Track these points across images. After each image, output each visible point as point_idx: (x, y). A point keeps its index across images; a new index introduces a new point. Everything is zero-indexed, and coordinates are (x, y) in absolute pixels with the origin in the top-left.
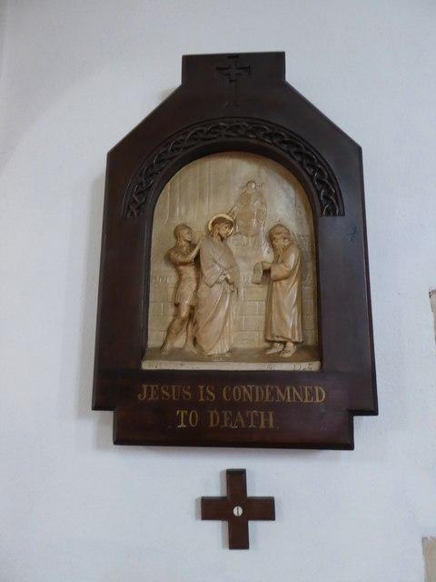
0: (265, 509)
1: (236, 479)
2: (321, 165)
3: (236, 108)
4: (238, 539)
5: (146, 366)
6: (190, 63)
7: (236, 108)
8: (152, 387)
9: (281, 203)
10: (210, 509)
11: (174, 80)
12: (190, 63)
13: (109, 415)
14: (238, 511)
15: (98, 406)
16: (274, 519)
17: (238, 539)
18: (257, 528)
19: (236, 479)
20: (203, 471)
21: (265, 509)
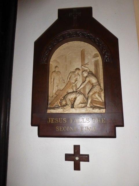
0: (86, 158)
1: (77, 148)
2: (108, 46)
3: (77, 24)
4: (77, 167)
5: (49, 111)
6: (61, 12)
8: (52, 119)
10: (68, 157)
11: (54, 17)
12: (61, 12)
13: (36, 128)
14: (77, 158)
15: (33, 124)
17: (77, 167)
18: (72, 163)
19: (77, 148)
20: (67, 145)
21: (86, 158)
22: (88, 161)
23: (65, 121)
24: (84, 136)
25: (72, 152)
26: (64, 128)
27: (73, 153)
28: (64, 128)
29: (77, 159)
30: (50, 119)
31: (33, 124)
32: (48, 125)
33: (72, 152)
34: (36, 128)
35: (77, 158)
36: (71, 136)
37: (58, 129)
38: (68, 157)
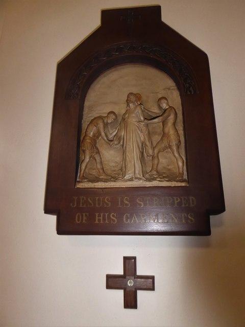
1: (130, 263)
2: (188, 69)
3: (134, 37)
4: (131, 302)
5: (79, 186)
6: (107, 15)
7: (134, 37)
9: (161, 87)
10: (112, 282)
11: (94, 23)
12: (107, 15)
13: (53, 219)
15: (47, 211)
16: (137, 308)
17: (131, 302)
18: (119, 294)
19: (130, 263)
20: (107, 252)
22: (153, 289)
23: (114, 221)
24: (160, 232)
25: (120, 272)
26: (77, 216)
27: (123, 274)
28: (77, 216)
29: (129, 285)
30: (76, 198)
31: (47, 211)
32: (76, 206)
33: (120, 272)
34: (53, 219)
35: (129, 284)
36: (112, 232)
37: (99, 219)
38: (112, 282)
